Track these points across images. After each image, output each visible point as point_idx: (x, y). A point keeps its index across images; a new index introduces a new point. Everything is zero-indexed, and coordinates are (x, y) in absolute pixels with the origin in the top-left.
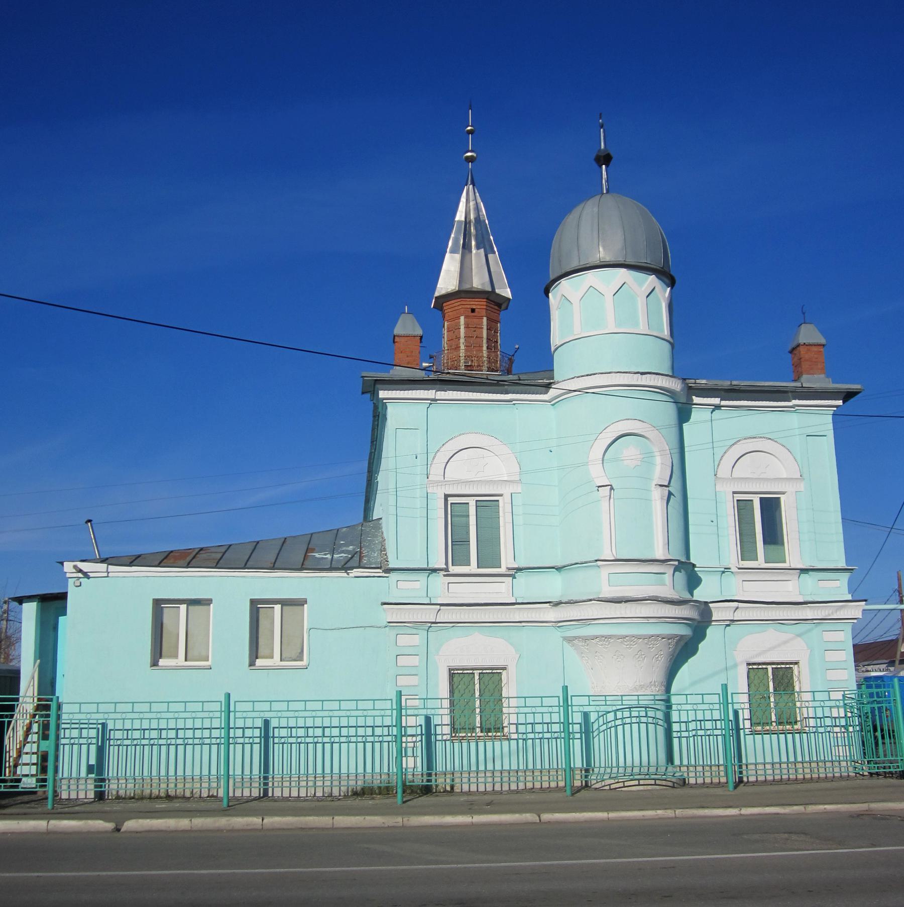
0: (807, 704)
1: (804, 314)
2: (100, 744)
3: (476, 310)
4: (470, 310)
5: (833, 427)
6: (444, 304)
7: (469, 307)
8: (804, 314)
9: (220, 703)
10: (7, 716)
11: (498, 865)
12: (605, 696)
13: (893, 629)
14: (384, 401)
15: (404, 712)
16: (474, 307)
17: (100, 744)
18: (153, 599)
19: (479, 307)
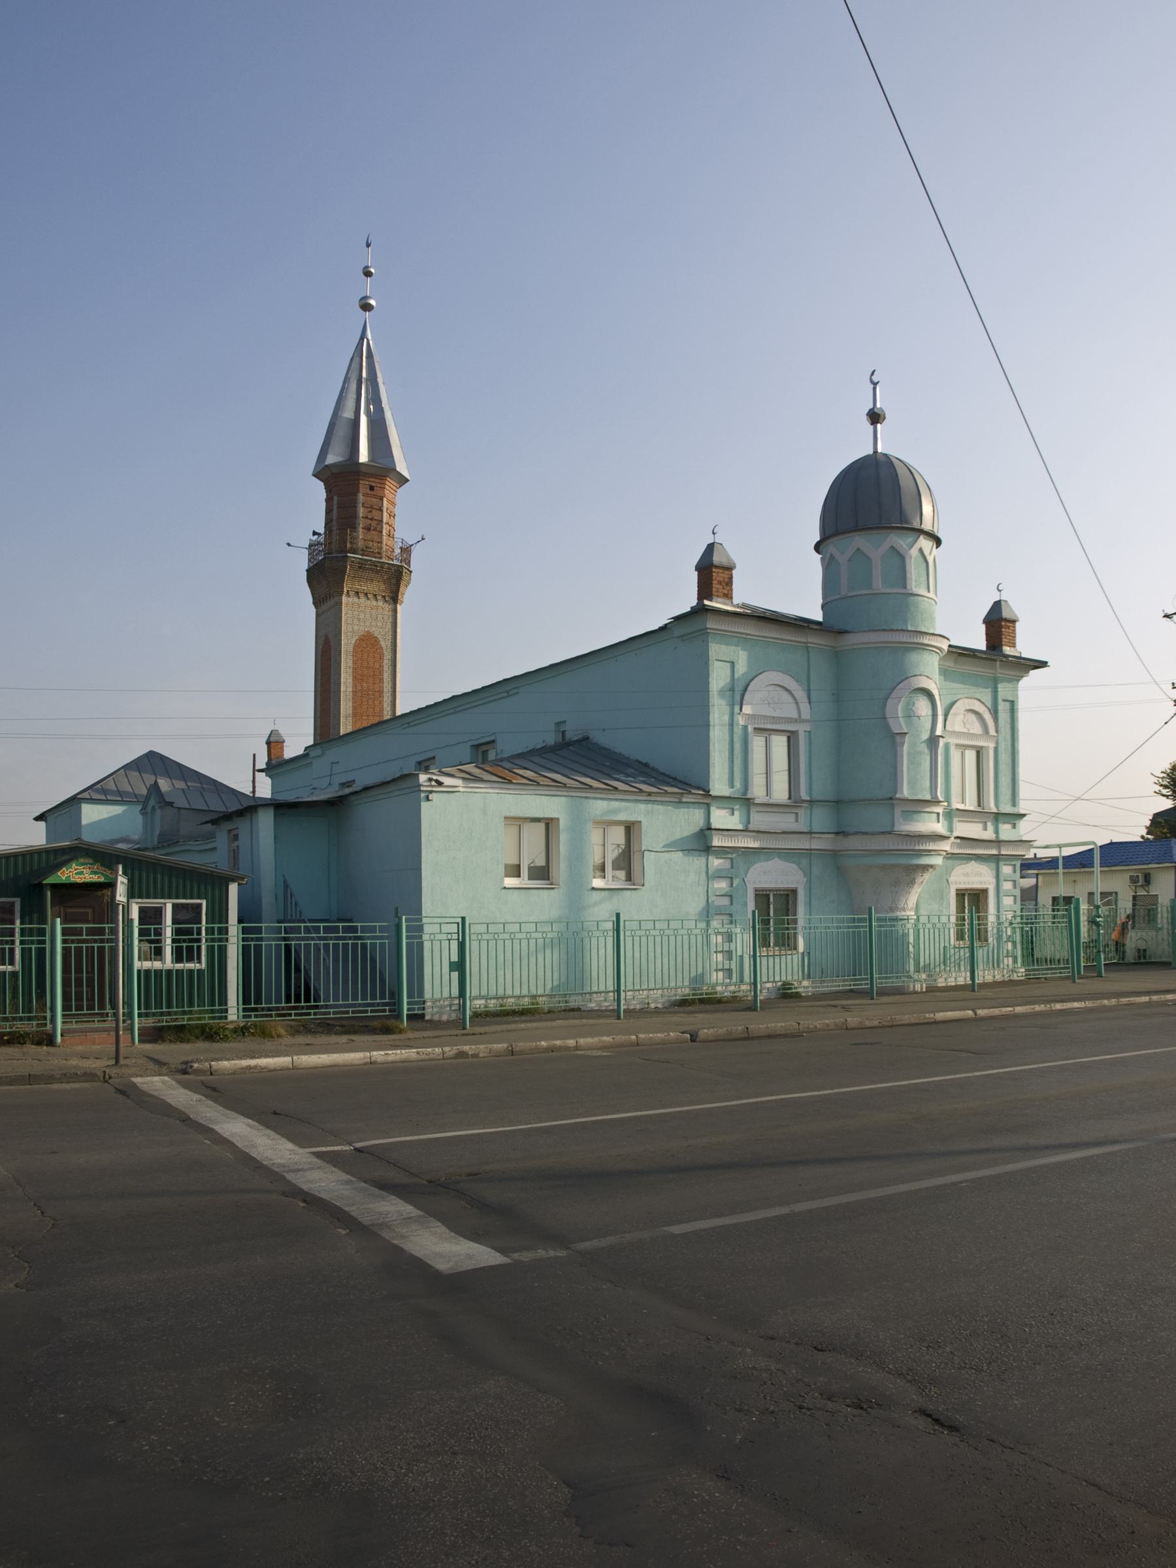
2: (460, 940)
3: (375, 488)
4: (368, 487)
5: (709, 709)
7: (367, 483)
9: (456, 925)
10: (7, 942)
16: (373, 484)
17: (460, 940)
18: (505, 865)
19: (378, 485)
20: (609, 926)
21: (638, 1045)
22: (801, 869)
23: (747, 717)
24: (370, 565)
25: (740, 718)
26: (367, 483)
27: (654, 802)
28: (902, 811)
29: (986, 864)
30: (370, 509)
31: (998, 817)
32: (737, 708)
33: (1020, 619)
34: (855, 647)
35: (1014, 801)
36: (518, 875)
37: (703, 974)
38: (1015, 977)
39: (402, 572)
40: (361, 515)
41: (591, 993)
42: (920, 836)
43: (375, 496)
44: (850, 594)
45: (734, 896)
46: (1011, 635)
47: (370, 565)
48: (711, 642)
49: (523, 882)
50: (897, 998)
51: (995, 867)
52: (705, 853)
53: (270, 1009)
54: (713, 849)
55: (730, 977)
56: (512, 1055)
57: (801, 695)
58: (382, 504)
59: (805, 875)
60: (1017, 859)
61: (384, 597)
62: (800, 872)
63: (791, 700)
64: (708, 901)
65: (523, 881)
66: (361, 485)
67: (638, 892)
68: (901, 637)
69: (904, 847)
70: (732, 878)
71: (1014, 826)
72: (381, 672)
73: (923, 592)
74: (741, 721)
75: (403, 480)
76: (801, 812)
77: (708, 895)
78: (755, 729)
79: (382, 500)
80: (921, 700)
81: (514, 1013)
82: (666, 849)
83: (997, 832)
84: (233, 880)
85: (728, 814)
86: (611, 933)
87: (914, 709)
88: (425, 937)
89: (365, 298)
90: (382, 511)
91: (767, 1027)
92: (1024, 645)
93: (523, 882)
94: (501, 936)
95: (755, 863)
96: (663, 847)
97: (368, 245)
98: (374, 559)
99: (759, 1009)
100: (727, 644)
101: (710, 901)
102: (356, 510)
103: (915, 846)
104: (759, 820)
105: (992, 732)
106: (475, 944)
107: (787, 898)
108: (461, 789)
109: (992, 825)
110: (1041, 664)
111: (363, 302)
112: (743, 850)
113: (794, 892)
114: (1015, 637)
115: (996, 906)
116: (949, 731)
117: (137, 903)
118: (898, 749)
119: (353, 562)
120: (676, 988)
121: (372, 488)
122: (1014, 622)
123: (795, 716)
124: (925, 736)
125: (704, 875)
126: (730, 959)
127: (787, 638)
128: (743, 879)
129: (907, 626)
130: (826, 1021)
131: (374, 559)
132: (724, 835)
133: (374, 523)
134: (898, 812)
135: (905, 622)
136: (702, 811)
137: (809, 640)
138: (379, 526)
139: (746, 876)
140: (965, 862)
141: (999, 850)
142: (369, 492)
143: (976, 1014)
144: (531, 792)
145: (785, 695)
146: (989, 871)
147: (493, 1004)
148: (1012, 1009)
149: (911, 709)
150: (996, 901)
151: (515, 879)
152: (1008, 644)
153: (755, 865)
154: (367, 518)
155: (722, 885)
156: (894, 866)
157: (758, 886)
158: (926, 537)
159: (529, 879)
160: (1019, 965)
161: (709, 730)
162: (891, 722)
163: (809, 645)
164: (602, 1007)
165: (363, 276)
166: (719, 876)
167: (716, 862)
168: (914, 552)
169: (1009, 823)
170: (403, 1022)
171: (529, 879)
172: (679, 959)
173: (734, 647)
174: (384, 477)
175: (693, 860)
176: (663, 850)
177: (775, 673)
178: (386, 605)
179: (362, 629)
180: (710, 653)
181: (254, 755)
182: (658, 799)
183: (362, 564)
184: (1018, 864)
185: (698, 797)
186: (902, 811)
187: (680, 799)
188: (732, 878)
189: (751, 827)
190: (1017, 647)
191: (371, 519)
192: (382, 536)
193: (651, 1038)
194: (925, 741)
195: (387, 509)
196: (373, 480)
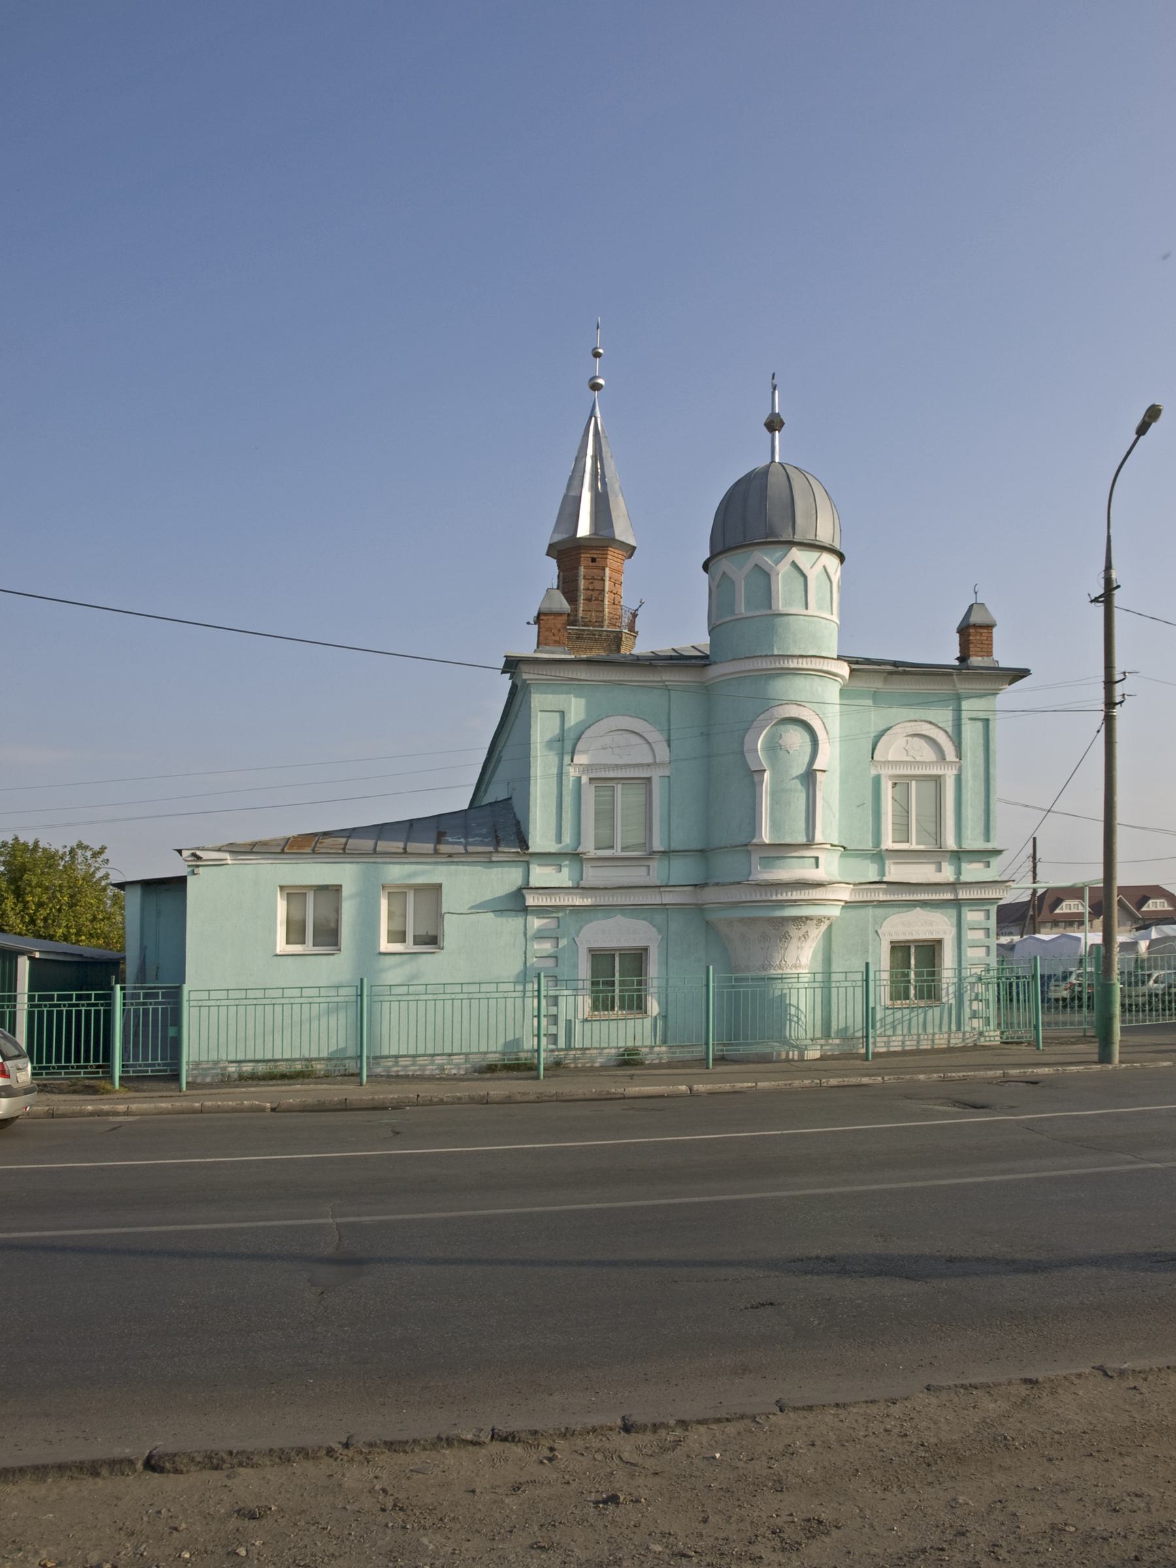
0: (948, 980)
1: (976, 593)
8: (976, 593)
10: (609, 991)
11: (313, 1221)
13: (1023, 895)
14: (528, 682)
15: (536, 993)
19: (600, 556)
20: (859, 977)
21: (201, 1112)
22: (654, 926)
23: (581, 768)
24: (588, 634)
25: (571, 770)
27: (457, 863)
28: (760, 858)
29: (941, 911)
30: (591, 581)
31: (958, 856)
32: (567, 759)
34: (717, 680)
36: (403, 940)
37: (846, 1028)
38: (982, 1041)
39: (621, 638)
40: (582, 587)
41: (397, 1057)
42: (772, 884)
43: (597, 567)
44: (718, 623)
45: (559, 957)
46: (987, 642)
47: (588, 634)
48: (535, 693)
49: (307, 949)
50: (760, 1067)
52: (522, 913)
53: (78, 1067)
54: (529, 908)
55: (555, 1043)
56: (53, 1118)
57: (655, 736)
58: (604, 573)
59: (659, 931)
60: (992, 904)
62: (654, 930)
63: (641, 741)
64: (525, 963)
65: (409, 946)
66: (582, 559)
67: (436, 956)
68: (782, 662)
69: (758, 898)
70: (557, 938)
71: (988, 865)
73: (797, 609)
74: (572, 772)
75: (630, 550)
76: (654, 864)
77: (525, 957)
78: (591, 779)
79: (604, 570)
80: (791, 731)
81: (283, 1076)
82: (473, 911)
83: (959, 872)
84: (22, 953)
85: (554, 871)
86: (860, 983)
87: (780, 742)
89: (595, 377)
90: (603, 580)
92: (1004, 655)
93: (307, 949)
94: (843, 984)
95: (591, 921)
96: (469, 909)
97: (598, 328)
98: (591, 628)
99: (542, 1077)
100: (554, 693)
101: (528, 965)
102: (577, 583)
103: (771, 896)
104: (592, 875)
105: (951, 755)
106: (194, 1011)
107: (637, 959)
108: (229, 862)
109: (950, 865)
110: (1023, 673)
111: (591, 382)
112: (571, 908)
113: (939, 942)
114: (992, 644)
115: (956, 959)
116: (878, 761)
118: (757, 788)
119: (570, 633)
121: (593, 560)
122: (990, 627)
123: (650, 760)
124: (800, 768)
125: (522, 936)
126: (556, 1023)
128: (574, 939)
129: (773, 650)
130: (458, 1094)
131: (591, 628)
132: (540, 894)
133: (595, 594)
134: (755, 858)
135: (771, 647)
136: (521, 869)
137: (664, 679)
138: (601, 596)
139: (578, 936)
140: (906, 909)
141: (956, 894)
142: (591, 564)
143: (691, 1090)
144: (309, 861)
145: (635, 739)
146: (946, 919)
147: (261, 1068)
148: (754, 1084)
149: (777, 743)
150: (956, 954)
151: (399, 944)
152: (980, 654)
153: (590, 925)
154: (588, 589)
155: (547, 947)
156: (754, 920)
157: (895, 938)
158: (799, 548)
159: (314, 945)
160: (992, 1028)
161: (529, 784)
162: (748, 757)
163: (667, 683)
164: (408, 1071)
165: (592, 357)
166: (540, 936)
167: (536, 923)
168: (784, 568)
169: (979, 862)
170: (113, 1083)
171: (314, 945)
172: (492, 1021)
173: (565, 696)
175: (507, 921)
176: (470, 911)
177: (619, 718)
180: (532, 705)
182: (463, 859)
183: (579, 634)
184: (993, 910)
185: (511, 855)
186: (760, 858)
187: (490, 858)
188: (557, 938)
189: (583, 884)
190: (994, 656)
191: (593, 590)
192: (603, 605)
193: (219, 1106)
194: (797, 777)
195: (610, 578)
196: (595, 552)
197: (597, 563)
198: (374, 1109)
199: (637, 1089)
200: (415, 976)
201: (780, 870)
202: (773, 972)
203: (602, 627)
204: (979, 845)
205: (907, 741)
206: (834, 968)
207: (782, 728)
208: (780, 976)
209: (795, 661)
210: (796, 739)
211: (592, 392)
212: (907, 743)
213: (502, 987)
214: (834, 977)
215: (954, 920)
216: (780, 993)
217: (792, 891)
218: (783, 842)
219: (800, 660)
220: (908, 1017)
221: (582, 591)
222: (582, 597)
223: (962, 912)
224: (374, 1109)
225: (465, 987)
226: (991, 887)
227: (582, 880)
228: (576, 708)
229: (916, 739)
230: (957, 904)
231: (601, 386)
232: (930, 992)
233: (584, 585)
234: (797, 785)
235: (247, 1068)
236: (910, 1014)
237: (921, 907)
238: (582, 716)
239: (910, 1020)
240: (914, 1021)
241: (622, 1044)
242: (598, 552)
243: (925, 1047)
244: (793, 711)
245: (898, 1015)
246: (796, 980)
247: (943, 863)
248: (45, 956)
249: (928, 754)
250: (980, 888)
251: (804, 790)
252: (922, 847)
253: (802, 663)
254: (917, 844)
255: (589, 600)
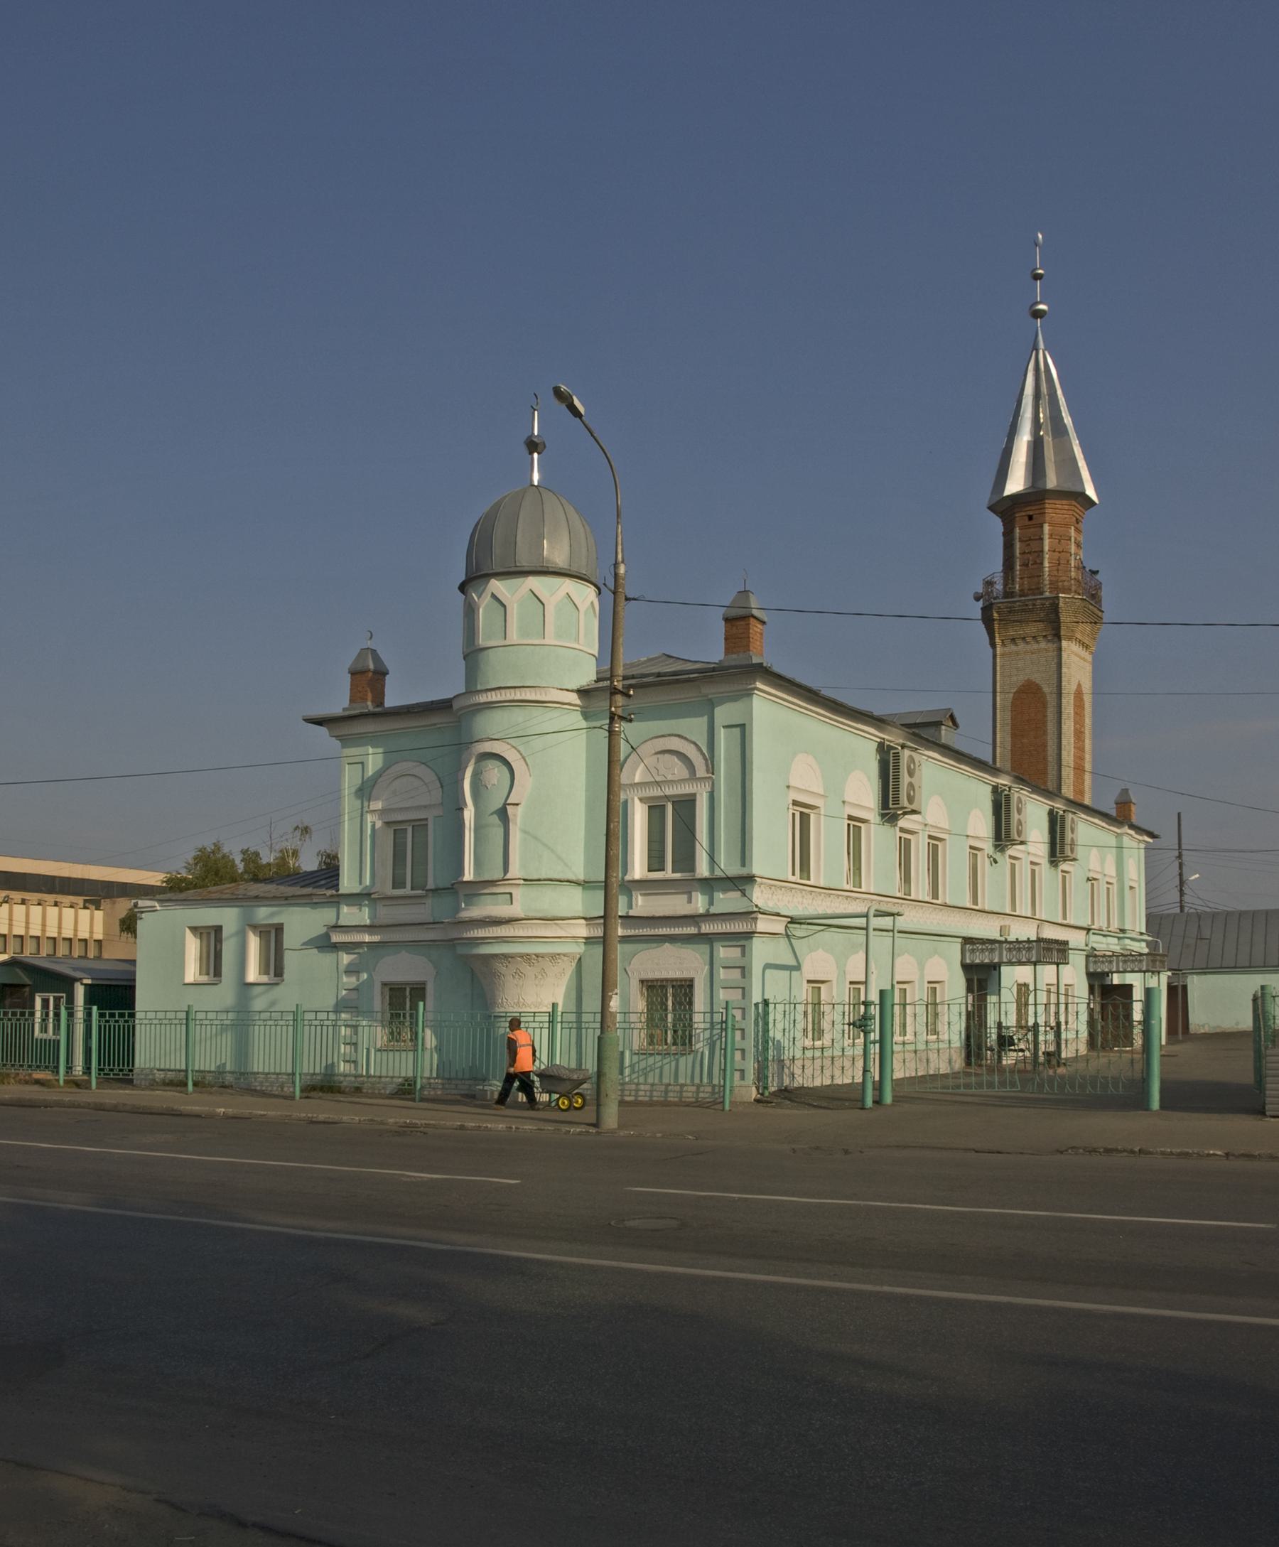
3: (1034, 516)
6: (1047, 501)
7: (1024, 514)
9: (292, 1014)
12: (534, 1013)
16: (1031, 513)
19: (1037, 512)
22: (431, 961)
24: (1019, 606)
26: (1024, 514)
33: (390, 673)
35: (744, 855)
39: (1058, 604)
51: (708, 951)
58: (1042, 531)
61: (1045, 636)
66: (1017, 519)
72: (1044, 723)
79: (1042, 527)
83: (711, 903)
86: (546, 1025)
87: (481, 778)
88: (137, 1022)
91: (445, 1124)
96: (302, 945)
105: (701, 772)
107: (418, 991)
108: (158, 908)
117: (39, 996)
120: (429, 1078)
127: (414, 725)
135: (476, 685)
140: (655, 945)
141: (700, 928)
146: (698, 956)
174: (1042, 500)
176: (301, 948)
178: (1050, 645)
179: (1019, 679)
181: (1179, 814)
183: (1010, 608)
191: (1030, 553)
194: (495, 812)
197: (1035, 522)
198: (173, 1115)
199: (190, 1108)
200: (273, 1003)
201: (475, 907)
202: (497, 1010)
203: (1042, 593)
204: (734, 870)
205: (658, 759)
206: (585, 1009)
207: (484, 763)
208: (504, 1014)
209: (485, 695)
210: (495, 773)
211: (1034, 320)
212: (658, 761)
213: (322, 1016)
214: (585, 1018)
215: (707, 958)
216: (503, 1032)
217: (477, 929)
218: (483, 879)
219: (489, 694)
220: (660, 1064)
221: (1018, 555)
222: (1018, 563)
223: (715, 948)
224: (173, 1115)
225: (262, 1014)
226: (708, 920)
227: (632, 908)
228: (373, 759)
229: (667, 756)
230: (709, 939)
231: (1043, 311)
232: (684, 1038)
233: (1020, 548)
234: (495, 819)
235: (170, 1075)
236: (662, 1060)
237: (671, 943)
238: (380, 764)
239: (661, 1068)
240: (666, 1068)
241: (403, 1074)
242: (1033, 508)
243: (672, 1099)
244: (488, 747)
245: (651, 1060)
246: (532, 1019)
247: (693, 893)
248: (95, 982)
249: (679, 770)
250: (724, 920)
251: (502, 825)
252: (678, 876)
253: (492, 697)
254: (673, 871)
255: (1025, 565)
